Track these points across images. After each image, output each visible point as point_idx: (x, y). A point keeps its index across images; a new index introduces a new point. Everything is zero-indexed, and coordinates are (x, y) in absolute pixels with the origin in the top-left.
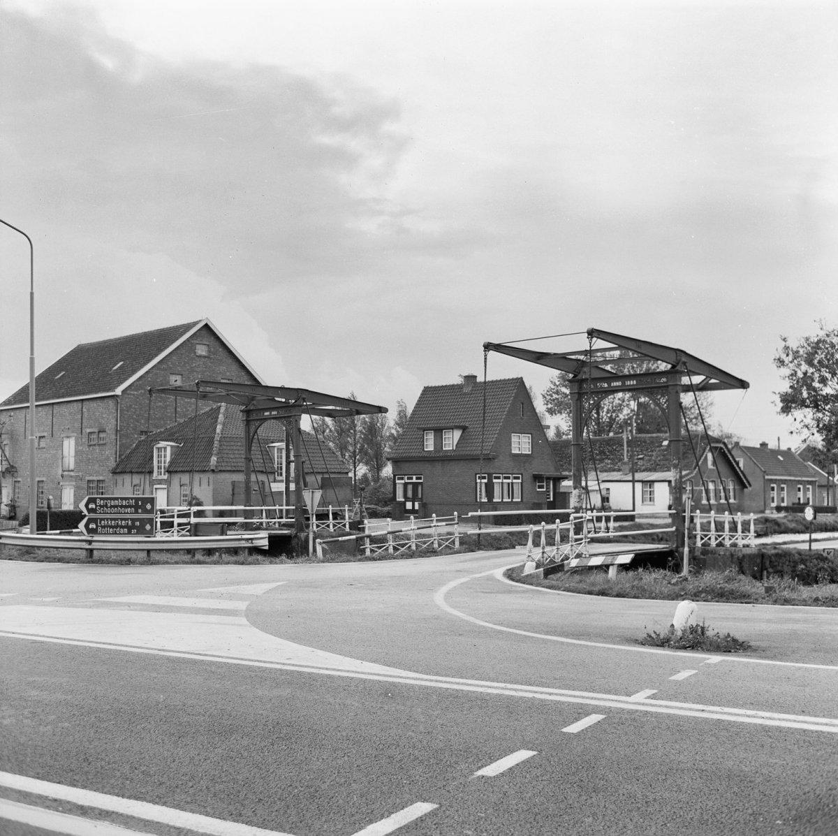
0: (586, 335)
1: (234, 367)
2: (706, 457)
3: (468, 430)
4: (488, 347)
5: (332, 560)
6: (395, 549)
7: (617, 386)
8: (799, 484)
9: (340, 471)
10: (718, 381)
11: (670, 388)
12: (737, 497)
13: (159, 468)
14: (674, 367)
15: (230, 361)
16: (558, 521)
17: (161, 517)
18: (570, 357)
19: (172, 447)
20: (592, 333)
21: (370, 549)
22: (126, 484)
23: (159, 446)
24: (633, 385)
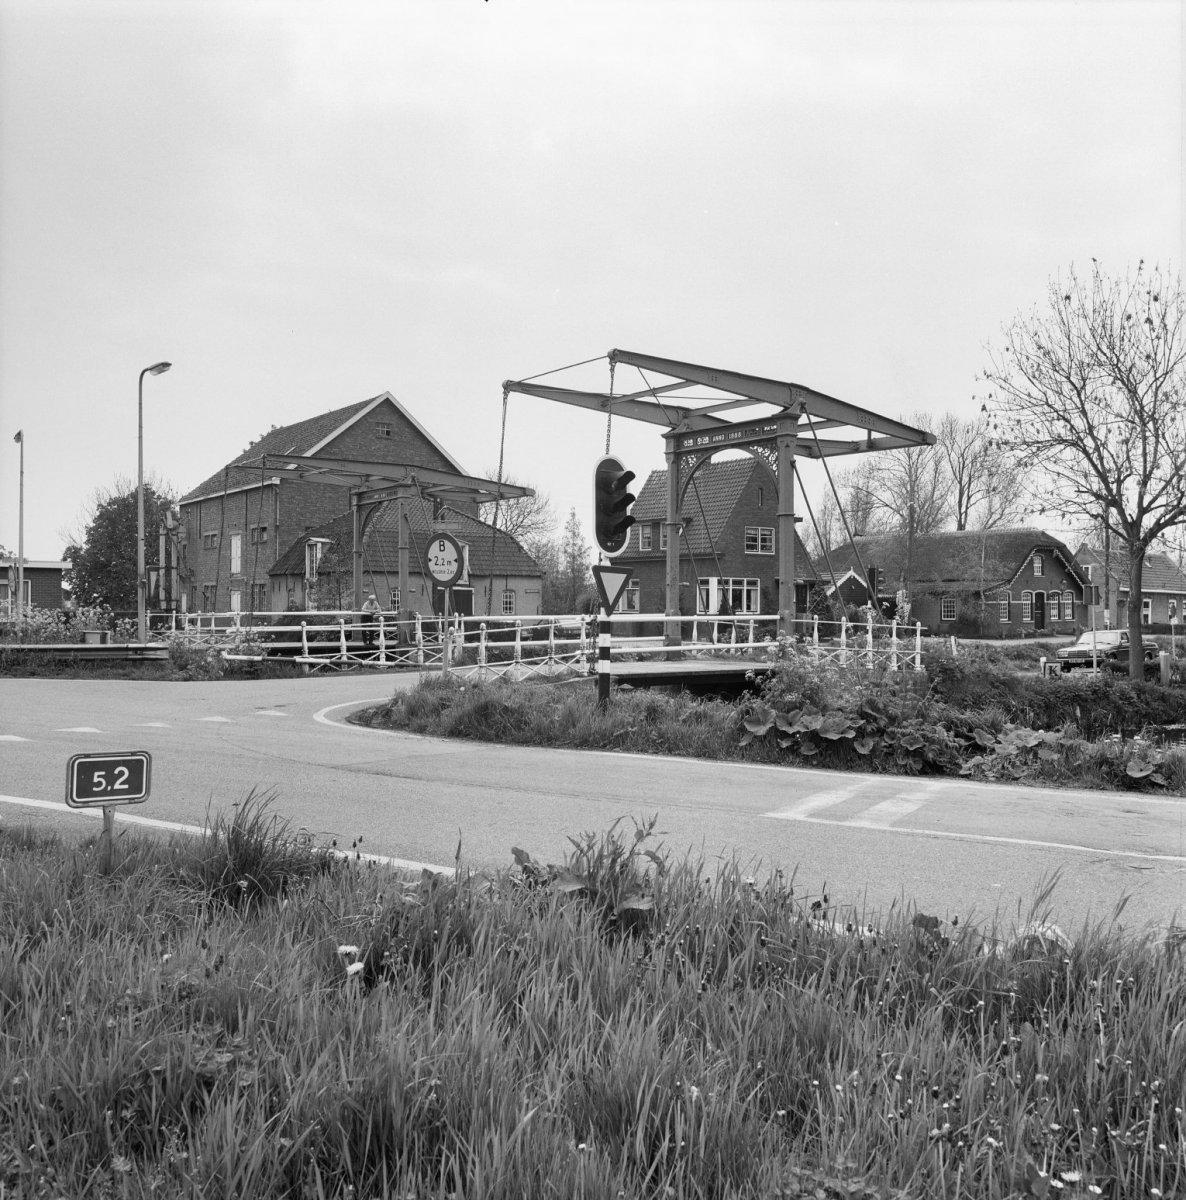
0: (608, 360)
1: (425, 451)
2: (1031, 562)
3: (692, 523)
4: (509, 387)
5: (742, 670)
6: (427, 657)
7: (719, 441)
8: (1146, 597)
9: (529, 573)
10: (885, 436)
11: (779, 440)
12: (1076, 616)
13: (311, 569)
14: (786, 408)
15: (419, 443)
16: (304, 623)
17: (443, 623)
18: (822, 420)
19: (323, 543)
20: (617, 356)
21: (387, 655)
22: (282, 589)
23: (310, 542)
24: (738, 438)
